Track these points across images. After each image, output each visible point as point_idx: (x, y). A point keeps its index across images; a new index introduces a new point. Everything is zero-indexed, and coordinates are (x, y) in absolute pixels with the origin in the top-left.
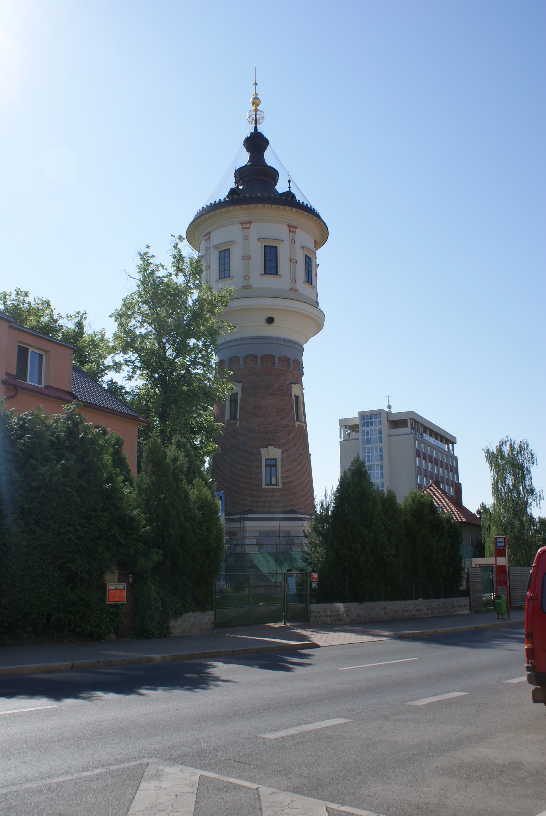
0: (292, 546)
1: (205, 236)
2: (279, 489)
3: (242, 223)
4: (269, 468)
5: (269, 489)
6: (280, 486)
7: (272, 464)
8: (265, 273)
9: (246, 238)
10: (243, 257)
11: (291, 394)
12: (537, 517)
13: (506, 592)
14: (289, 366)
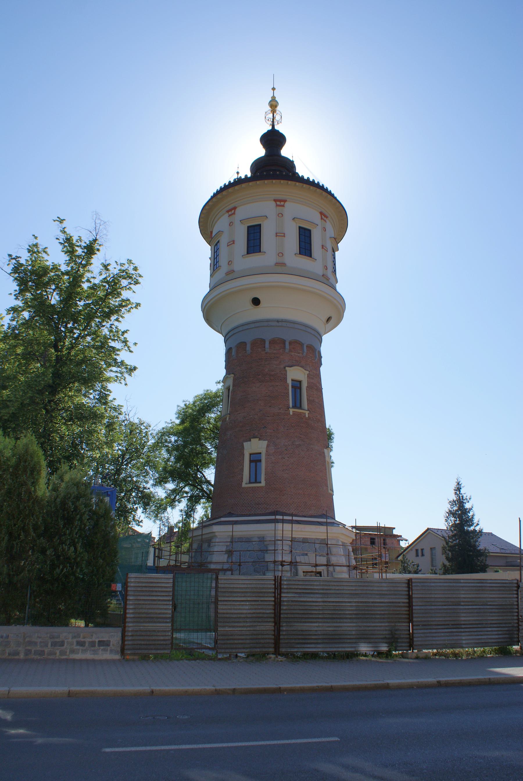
0: (265, 554)
1: (228, 211)
3: (275, 201)
4: (253, 464)
5: (250, 488)
6: (263, 484)
7: (255, 460)
8: (300, 254)
9: (281, 215)
10: (276, 233)
11: (285, 379)
13: (274, 582)
14: (284, 347)
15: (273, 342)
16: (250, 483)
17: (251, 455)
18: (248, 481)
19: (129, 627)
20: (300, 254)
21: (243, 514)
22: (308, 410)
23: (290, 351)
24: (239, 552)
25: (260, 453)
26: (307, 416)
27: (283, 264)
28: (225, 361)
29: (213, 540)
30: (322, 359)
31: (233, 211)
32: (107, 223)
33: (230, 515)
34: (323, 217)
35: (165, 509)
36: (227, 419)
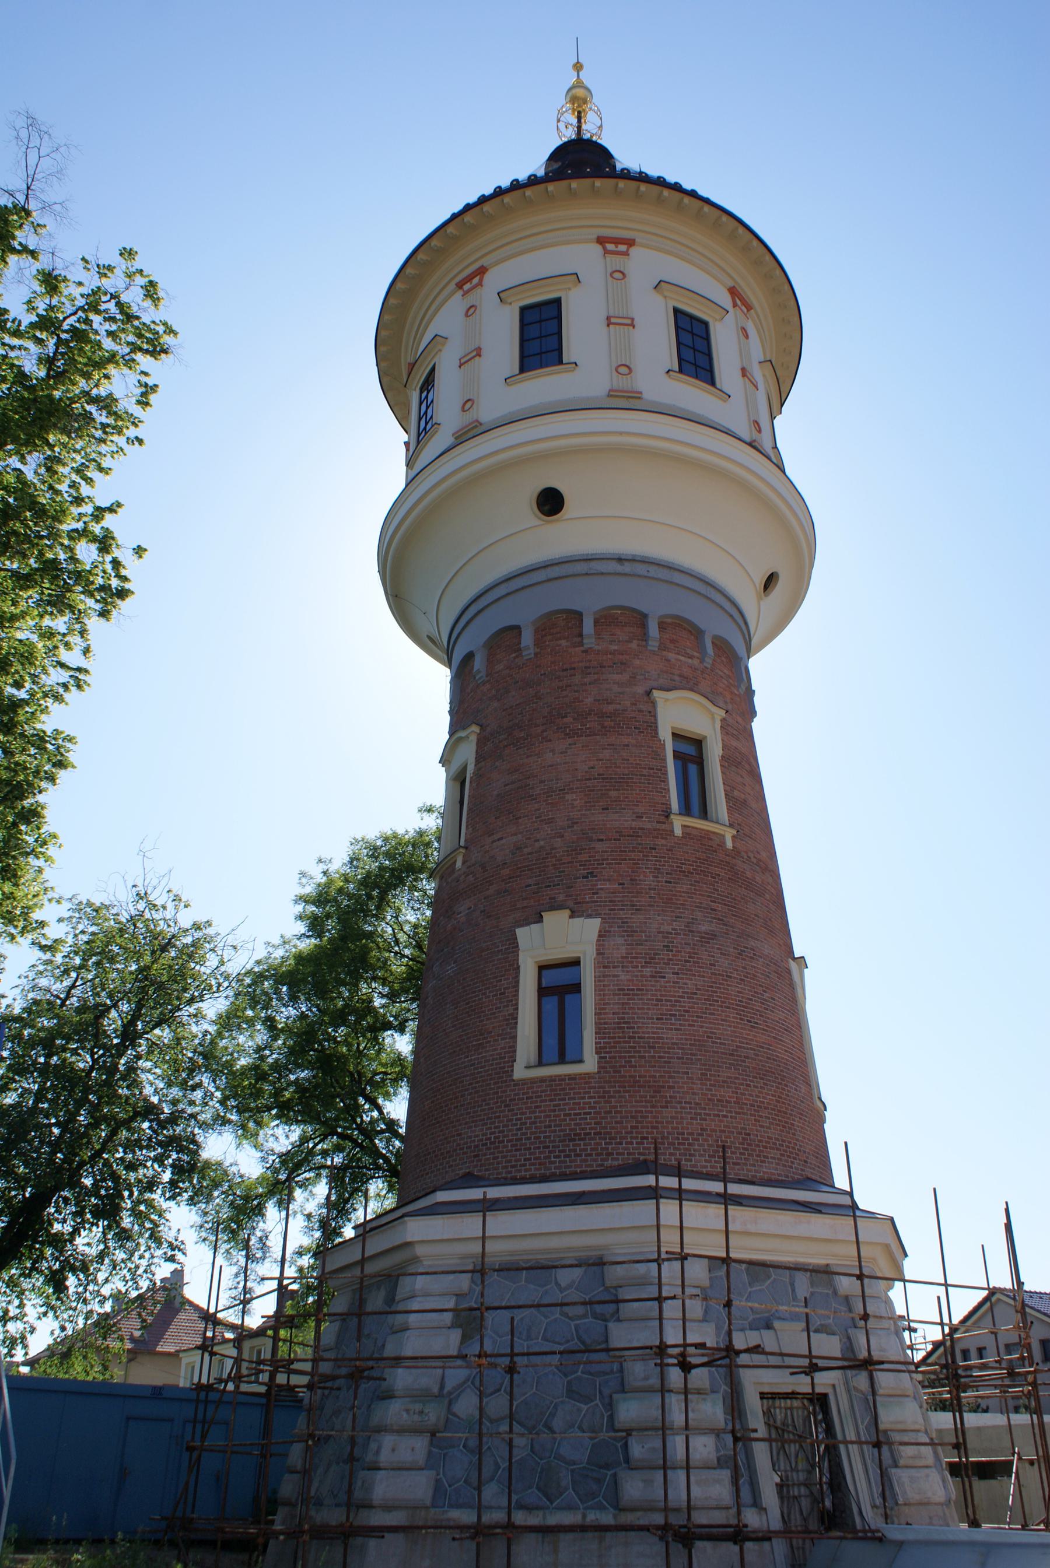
0: (611, 1325)
1: (460, 286)
2: (587, 1076)
3: (601, 241)
4: (551, 1003)
5: (542, 1080)
6: (590, 1064)
8: (681, 371)
10: (608, 318)
11: (651, 727)
12: (507, 308)
14: (644, 637)
15: (606, 619)
16: (540, 1063)
17: (544, 972)
18: (533, 1058)
19: (691, 1356)
20: (681, 371)
21: (518, 1175)
22: (731, 826)
23: (663, 647)
24: (507, 1314)
25: (576, 963)
26: (729, 844)
27: (637, 395)
28: (451, 703)
29: (405, 1285)
30: (756, 699)
31: (476, 280)
32: (63, 150)
33: (469, 1180)
34: (739, 302)
35: (259, 1211)
36: (459, 864)
